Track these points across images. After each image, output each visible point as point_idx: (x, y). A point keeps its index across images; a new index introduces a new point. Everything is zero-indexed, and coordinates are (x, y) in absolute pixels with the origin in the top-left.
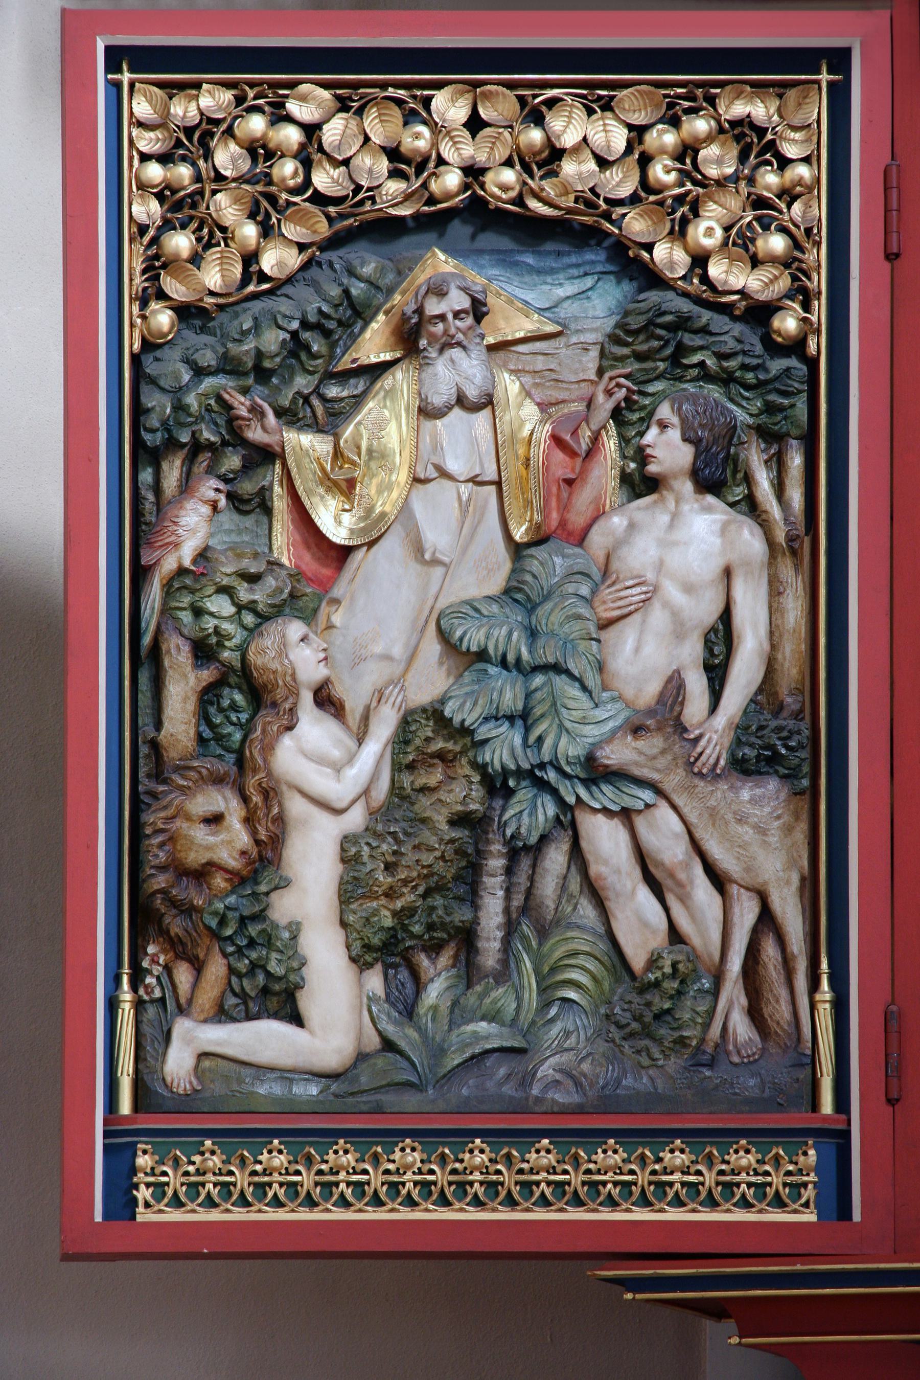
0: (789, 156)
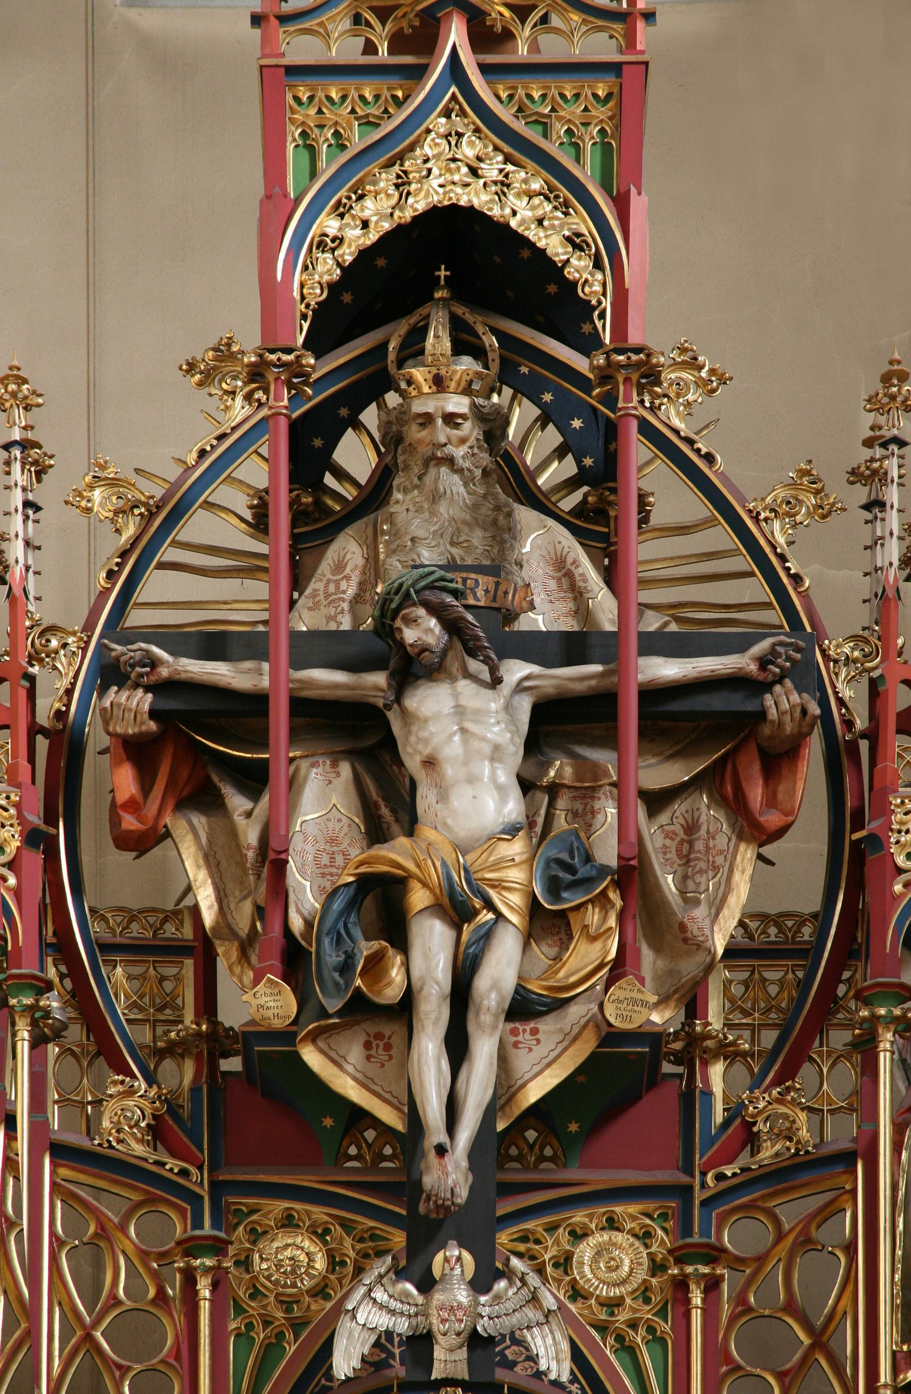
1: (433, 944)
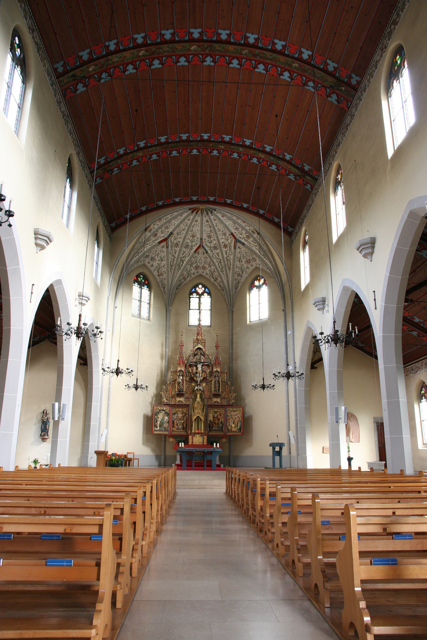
0: (119, 579)
1: (198, 374)
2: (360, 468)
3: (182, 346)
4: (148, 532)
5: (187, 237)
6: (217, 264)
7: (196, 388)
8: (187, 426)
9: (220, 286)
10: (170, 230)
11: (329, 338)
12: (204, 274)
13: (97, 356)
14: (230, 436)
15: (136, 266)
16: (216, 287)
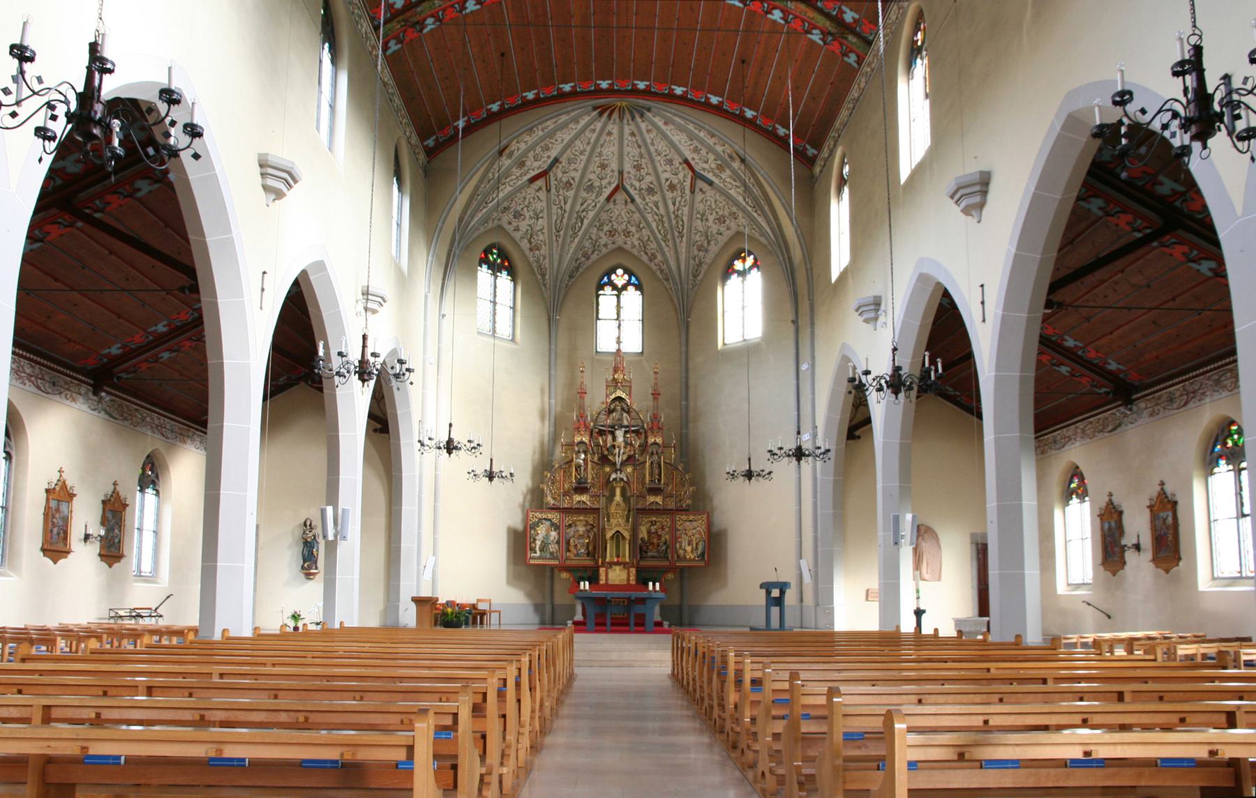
2: (936, 630)
3: (582, 393)
4: (512, 752)
5: (591, 168)
6: (654, 225)
7: (613, 476)
8: (596, 548)
9: (662, 271)
10: (553, 154)
11: (883, 382)
12: (628, 247)
13: (408, 415)
14: (682, 569)
15: (482, 229)
16: (654, 273)
